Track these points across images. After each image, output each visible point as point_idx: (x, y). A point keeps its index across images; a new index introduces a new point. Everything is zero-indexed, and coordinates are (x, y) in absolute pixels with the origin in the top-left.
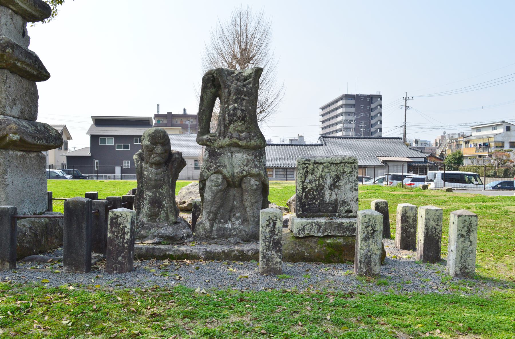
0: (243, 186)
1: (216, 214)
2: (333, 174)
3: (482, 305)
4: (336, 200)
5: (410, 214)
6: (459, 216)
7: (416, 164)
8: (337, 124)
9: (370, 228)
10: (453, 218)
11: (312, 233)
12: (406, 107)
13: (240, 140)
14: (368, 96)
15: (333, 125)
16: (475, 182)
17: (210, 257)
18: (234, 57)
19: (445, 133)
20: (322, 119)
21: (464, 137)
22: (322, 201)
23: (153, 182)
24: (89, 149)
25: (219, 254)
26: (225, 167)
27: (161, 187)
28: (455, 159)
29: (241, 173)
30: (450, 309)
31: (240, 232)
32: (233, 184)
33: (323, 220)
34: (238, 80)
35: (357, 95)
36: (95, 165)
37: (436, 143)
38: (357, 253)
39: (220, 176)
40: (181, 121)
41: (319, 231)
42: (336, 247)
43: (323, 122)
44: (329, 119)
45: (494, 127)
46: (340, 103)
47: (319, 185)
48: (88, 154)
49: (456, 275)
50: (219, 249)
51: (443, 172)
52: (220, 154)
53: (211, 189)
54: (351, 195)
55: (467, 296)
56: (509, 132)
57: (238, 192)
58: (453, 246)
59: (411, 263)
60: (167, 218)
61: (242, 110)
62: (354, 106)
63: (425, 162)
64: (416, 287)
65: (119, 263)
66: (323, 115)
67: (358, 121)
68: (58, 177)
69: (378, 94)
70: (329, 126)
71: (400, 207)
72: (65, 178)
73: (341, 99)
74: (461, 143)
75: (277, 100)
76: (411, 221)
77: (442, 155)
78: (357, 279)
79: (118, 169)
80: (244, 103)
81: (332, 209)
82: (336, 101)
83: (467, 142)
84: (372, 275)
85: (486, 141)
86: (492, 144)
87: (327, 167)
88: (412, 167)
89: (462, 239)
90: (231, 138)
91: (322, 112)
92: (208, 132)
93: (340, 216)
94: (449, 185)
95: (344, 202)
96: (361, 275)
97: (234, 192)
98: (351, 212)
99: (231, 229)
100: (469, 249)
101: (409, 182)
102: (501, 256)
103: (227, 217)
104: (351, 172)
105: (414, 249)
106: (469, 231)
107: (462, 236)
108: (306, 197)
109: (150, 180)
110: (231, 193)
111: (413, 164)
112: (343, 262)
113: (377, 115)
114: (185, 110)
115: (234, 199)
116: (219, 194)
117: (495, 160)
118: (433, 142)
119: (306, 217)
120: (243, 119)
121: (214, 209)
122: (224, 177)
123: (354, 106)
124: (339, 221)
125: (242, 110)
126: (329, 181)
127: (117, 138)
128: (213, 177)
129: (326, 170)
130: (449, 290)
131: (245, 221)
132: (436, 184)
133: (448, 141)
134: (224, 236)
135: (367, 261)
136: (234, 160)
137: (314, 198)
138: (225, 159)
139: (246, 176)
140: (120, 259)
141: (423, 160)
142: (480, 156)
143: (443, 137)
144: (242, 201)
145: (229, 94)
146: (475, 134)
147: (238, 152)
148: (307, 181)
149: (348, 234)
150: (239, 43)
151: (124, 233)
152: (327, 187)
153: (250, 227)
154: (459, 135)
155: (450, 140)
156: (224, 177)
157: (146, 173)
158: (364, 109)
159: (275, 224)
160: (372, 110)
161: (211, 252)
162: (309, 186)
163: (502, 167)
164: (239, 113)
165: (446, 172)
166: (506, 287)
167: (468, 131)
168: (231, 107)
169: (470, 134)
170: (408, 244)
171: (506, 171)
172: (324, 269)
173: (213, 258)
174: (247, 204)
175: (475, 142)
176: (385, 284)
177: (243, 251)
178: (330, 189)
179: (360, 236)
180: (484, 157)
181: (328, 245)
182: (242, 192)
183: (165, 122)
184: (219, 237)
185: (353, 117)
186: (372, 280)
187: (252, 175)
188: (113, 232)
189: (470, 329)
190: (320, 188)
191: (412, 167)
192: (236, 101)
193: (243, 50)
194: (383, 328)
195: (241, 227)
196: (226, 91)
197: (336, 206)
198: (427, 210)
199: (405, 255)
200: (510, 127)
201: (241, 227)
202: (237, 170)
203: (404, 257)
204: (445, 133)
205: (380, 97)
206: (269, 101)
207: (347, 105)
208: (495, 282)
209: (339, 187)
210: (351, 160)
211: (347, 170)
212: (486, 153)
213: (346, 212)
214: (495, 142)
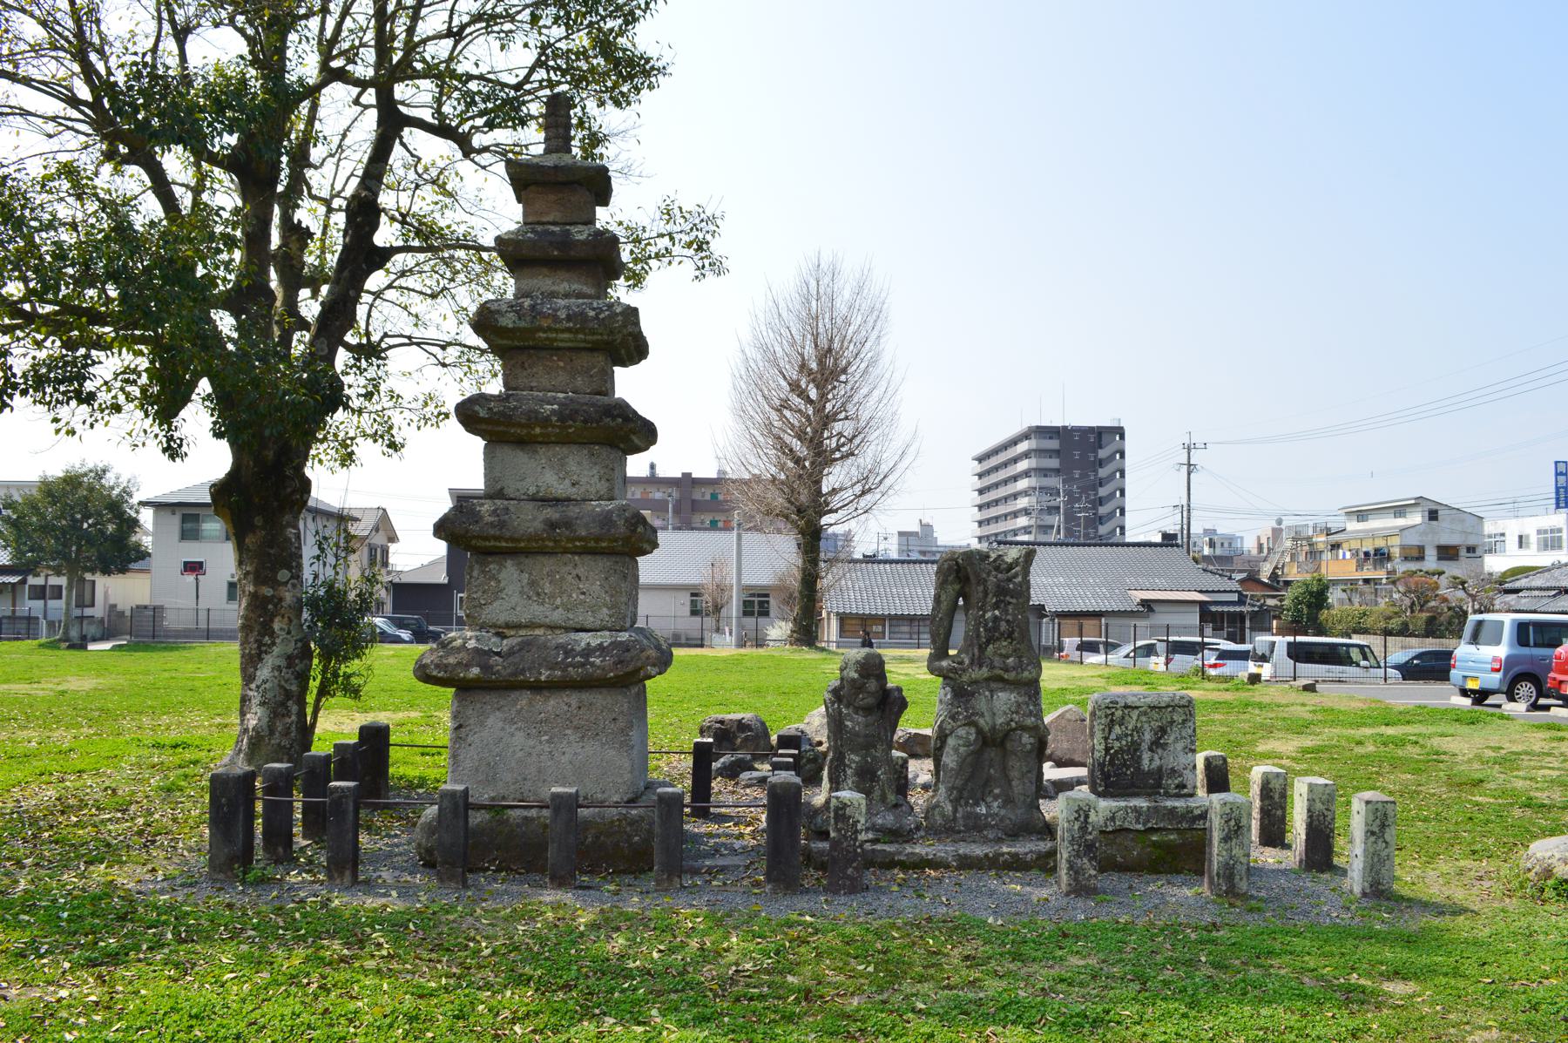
0: (1009, 745)
1: (960, 791)
2: (1155, 724)
3: (1409, 941)
4: (1160, 768)
5: (1276, 785)
6: (1368, 802)
7: (1220, 609)
8: (1015, 496)
9: (1232, 823)
10: (1357, 805)
11: (1126, 825)
12: (1190, 468)
13: (1007, 670)
14: (1091, 429)
15: (1006, 499)
16: (1363, 663)
17: (966, 863)
18: (803, 366)
19: (1279, 522)
20: (979, 484)
22: (1138, 769)
23: (861, 740)
24: (445, 566)
25: (978, 859)
26: (982, 715)
27: (875, 747)
28: (1311, 593)
29: (1008, 724)
30: (1365, 948)
31: (1002, 820)
32: (993, 742)
33: (1142, 803)
34: (997, 569)
35: (1065, 428)
37: (1260, 547)
38: (1210, 861)
39: (973, 730)
40: (645, 492)
41: (1138, 822)
42: (1167, 847)
43: (981, 492)
44: (996, 485)
45: (1400, 511)
46: (1023, 447)
47: (1133, 742)
48: (441, 577)
49: (1364, 894)
50: (978, 850)
51: (1291, 639)
52: (973, 694)
53: (956, 750)
54: (1183, 759)
55: (1384, 928)
57: (999, 756)
58: (1359, 849)
59: (1284, 872)
60: (883, 799)
61: (1008, 621)
62: (1057, 471)
63: (1241, 602)
64: (1306, 913)
65: (848, 877)
66: (980, 476)
67: (1072, 499)
68: (386, 638)
70: (996, 502)
71: (1257, 772)
72: (398, 640)
73: (1025, 436)
74: (1321, 547)
75: (902, 466)
76: (1277, 796)
77: (1274, 576)
78: (1214, 902)
80: (1010, 608)
81: (1153, 783)
82: (1014, 442)
83: (1336, 546)
84: (1237, 896)
85: (1380, 543)
86: (1396, 552)
87: (1145, 713)
88: (1210, 616)
89: (1373, 839)
90: (992, 667)
91: (978, 468)
92: (947, 655)
93: (1168, 795)
94: (1310, 671)
95: (1173, 770)
96: (1219, 896)
97: (992, 753)
98: (1184, 786)
99: (986, 816)
100: (1384, 854)
101: (1213, 661)
102: (1432, 858)
103: (979, 795)
104: (1184, 721)
105: (843, 619)
106: (1383, 826)
107: (1373, 833)
108: (1112, 762)
109: (857, 735)
110: (986, 756)
111: (1213, 609)
112: (1178, 872)
114: (652, 466)
115: (991, 766)
116: (969, 759)
117: (1404, 594)
118: (1249, 545)
119: (1113, 796)
120: (1010, 635)
121: (959, 783)
122: (980, 731)
123: (1057, 471)
124: (1169, 803)
125: (1008, 621)
126: (1148, 737)
128: (962, 732)
129: (1144, 719)
130: (1357, 920)
131: (1008, 801)
132: (1275, 666)
133: (1289, 544)
134: (976, 827)
135: (1229, 872)
136: (996, 703)
137: (1124, 765)
138: (981, 703)
139: (1014, 730)
140: (850, 871)
141: (1235, 597)
142: (1367, 581)
143: (1277, 533)
144: (1004, 770)
145: (986, 593)
146: (1353, 526)
147: (1002, 690)
148: (1113, 736)
149: (1185, 825)
150: (816, 337)
151: (856, 832)
152: (1145, 746)
153: (1019, 812)
154: (1315, 528)
155: (1294, 539)
156: (980, 731)
157: (848, 723)
158: (1081, 463)
159: (1087, 817)
160: (1101, 463)
161: (966, 857)
162: (1117, 745)
163: (1421, 611)
164: (1003, 626)
165: (1300, 639)
166: (1442, 913)
168: (989, 615)
169: (1342, 526)
171: (1431, 621)
172: (1156, 886)
173: (970, 867)
174: (1014, 774)
175: (1355, 545)
176: (1259, 909)
177: (1017, 854)
178: (1151, 749)
179: (1216, 836)
180: (1376, 582)
181: (1154, 844)
182: (1005, 754)
184: (968, 829)
186: (1239, 903)
187: (1024, 728)
188: (838, 831)
189: (1396, 973)
190: (1134, 748)
191: (1210, 616)
192: (996, 606)
193: (825, 353)
194: (1283, 972)
195: (1003, 812)
196: (981, 588)
197: (1161, 778)
198: (1310, 785)
199: (1269, 857)
200: (1436, 512)
201: (1003, 812)
202: (1000, 720)
203: (1270, 860)
204: (1279, 522)
206: (884, 468)
207: (1039, 452)
208: (1425, 906)
209: (1164, 746)
210: (1183, 702)
211: (1178, 718)
212: (1381, 574)
213: (1177, 787)
214: (1403, 547)
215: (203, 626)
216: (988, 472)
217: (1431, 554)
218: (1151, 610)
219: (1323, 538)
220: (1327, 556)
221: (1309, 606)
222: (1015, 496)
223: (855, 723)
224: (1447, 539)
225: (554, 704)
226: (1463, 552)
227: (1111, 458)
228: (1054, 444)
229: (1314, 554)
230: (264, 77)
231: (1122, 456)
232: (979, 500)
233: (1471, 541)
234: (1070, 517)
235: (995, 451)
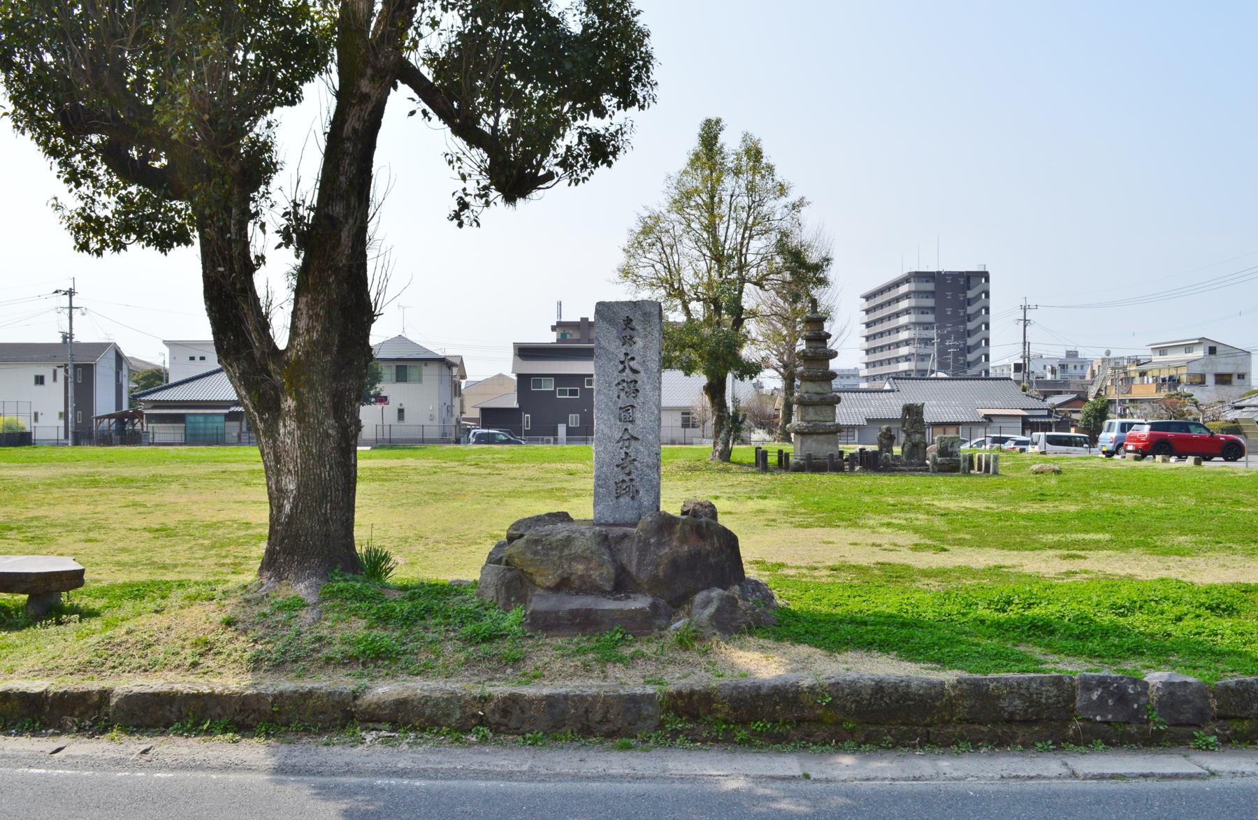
8: (897, 330)
14: (961, 274)
15: (889, 332)
19: (1108, 353)
20: (866, 319)
21: (1138, 362)
35: (939, 273)
36: (524, 423)
43: (868, 325)
45: (1188, 347)
46: (904, 289)
56: (1213, 357)
62: (933, 309)
63: (1049, 416)
66: (868, 311)
67: (943, 338)
69: (982, 270)
70: (881, 334)
73: (906, 280)
74: (1132, 374)
79: (562, 429)
81: (951, 454)
82: (897, 284)
83: (1143, 374)
85: (1173, 372)
86: (1184, 378)
91: (866, 305)
113: (978, 345)
123: (933, 309)
127: (560, 379)
134: (912, 464)
141: (1046, 413)
146: (1157, 358)
160: (969, 302)
167: (1144, 353)
170: (980, 469)
175: (1156, 373)
183: (576, 336)
185: (933, 333)
204: (1108, 353)
205: (985, 275)
215: (387, 437)
216: (874, 309)
217: (1210, 380)
218: (990, 421)
219: (1134, 368)
220: (1138, 380)
221: (1095, 418)
222: (897, 330)
223: (885, 441)
224: (1222, 369)
225: (822, 437)
226: (1235, 379)
227: (978, 297)
228: (930, 286)
229: (1128, 380)
230: (337, 22)
231: (987, 296)
232: (866, 332)
233: (1241, 371)
234: (942, 352)
235: (881, 291)
